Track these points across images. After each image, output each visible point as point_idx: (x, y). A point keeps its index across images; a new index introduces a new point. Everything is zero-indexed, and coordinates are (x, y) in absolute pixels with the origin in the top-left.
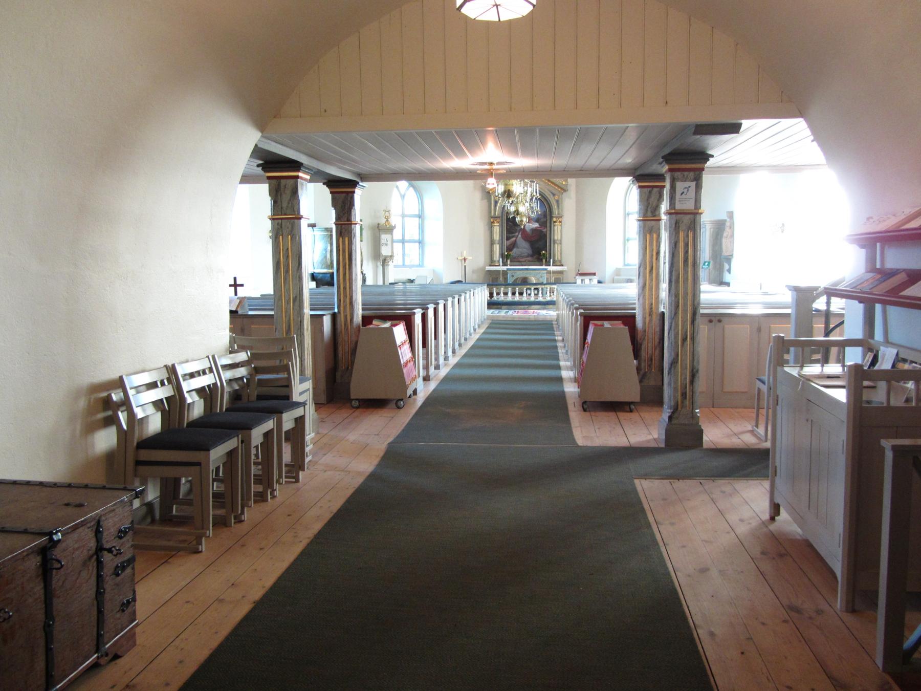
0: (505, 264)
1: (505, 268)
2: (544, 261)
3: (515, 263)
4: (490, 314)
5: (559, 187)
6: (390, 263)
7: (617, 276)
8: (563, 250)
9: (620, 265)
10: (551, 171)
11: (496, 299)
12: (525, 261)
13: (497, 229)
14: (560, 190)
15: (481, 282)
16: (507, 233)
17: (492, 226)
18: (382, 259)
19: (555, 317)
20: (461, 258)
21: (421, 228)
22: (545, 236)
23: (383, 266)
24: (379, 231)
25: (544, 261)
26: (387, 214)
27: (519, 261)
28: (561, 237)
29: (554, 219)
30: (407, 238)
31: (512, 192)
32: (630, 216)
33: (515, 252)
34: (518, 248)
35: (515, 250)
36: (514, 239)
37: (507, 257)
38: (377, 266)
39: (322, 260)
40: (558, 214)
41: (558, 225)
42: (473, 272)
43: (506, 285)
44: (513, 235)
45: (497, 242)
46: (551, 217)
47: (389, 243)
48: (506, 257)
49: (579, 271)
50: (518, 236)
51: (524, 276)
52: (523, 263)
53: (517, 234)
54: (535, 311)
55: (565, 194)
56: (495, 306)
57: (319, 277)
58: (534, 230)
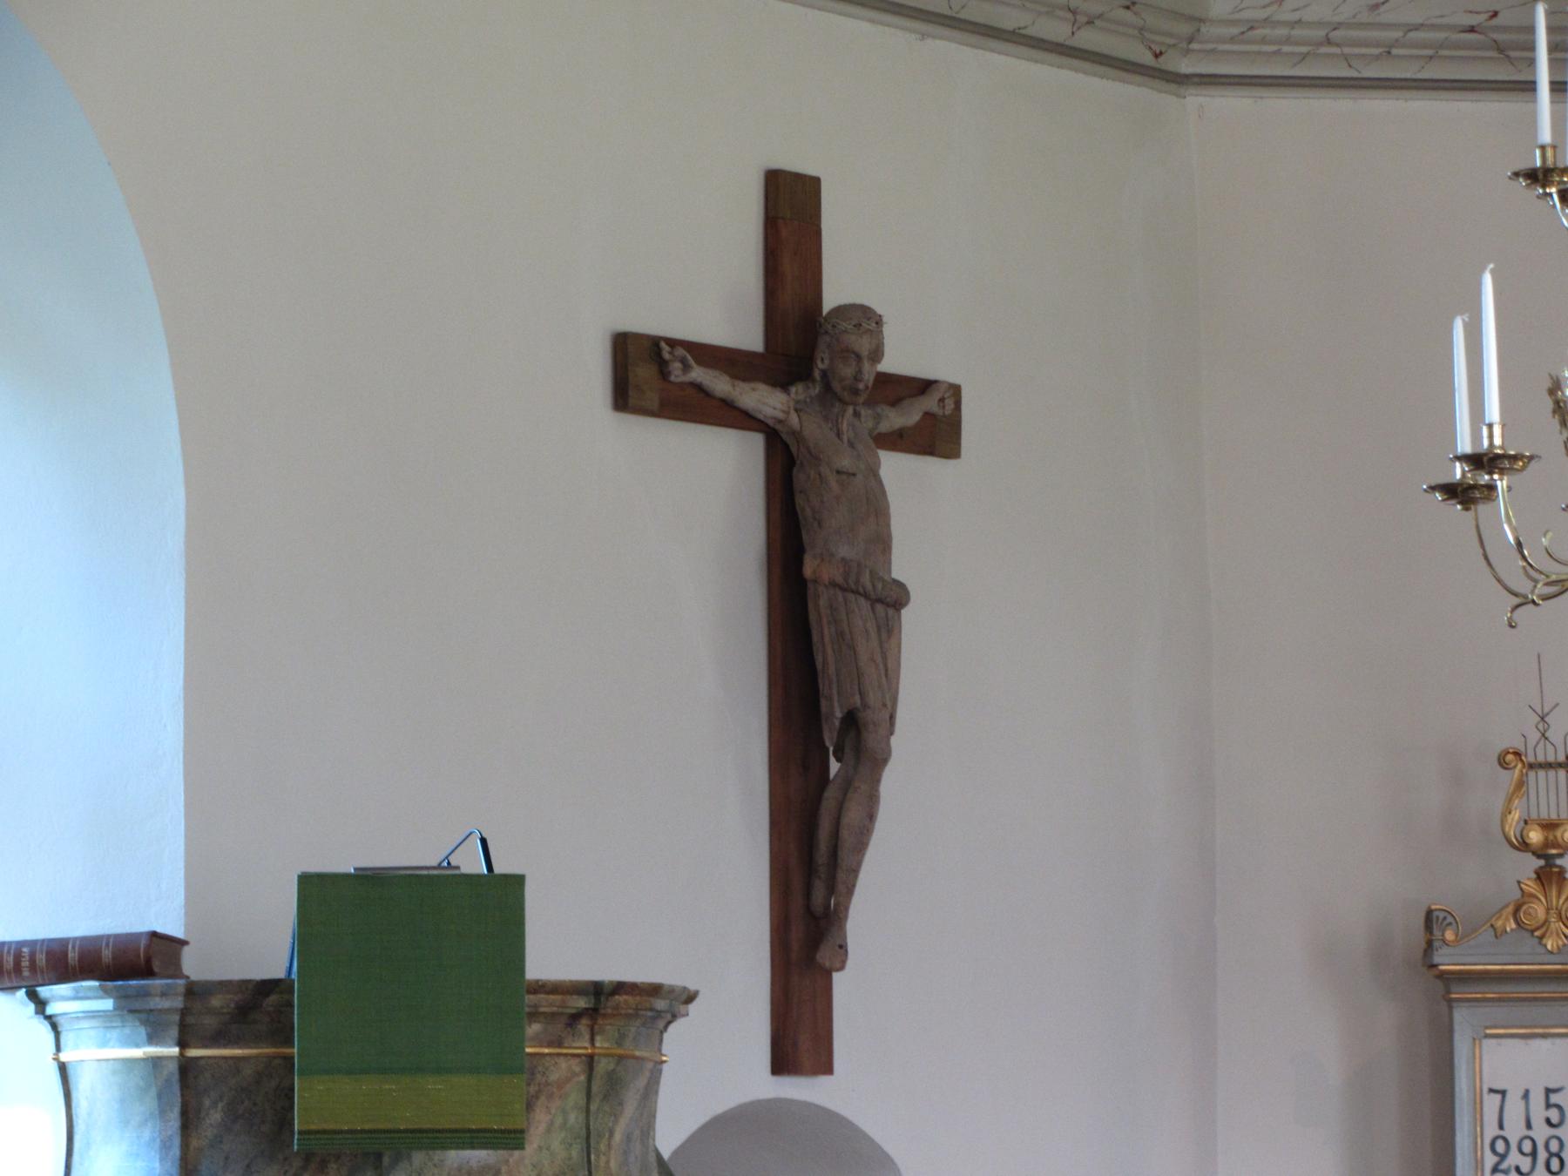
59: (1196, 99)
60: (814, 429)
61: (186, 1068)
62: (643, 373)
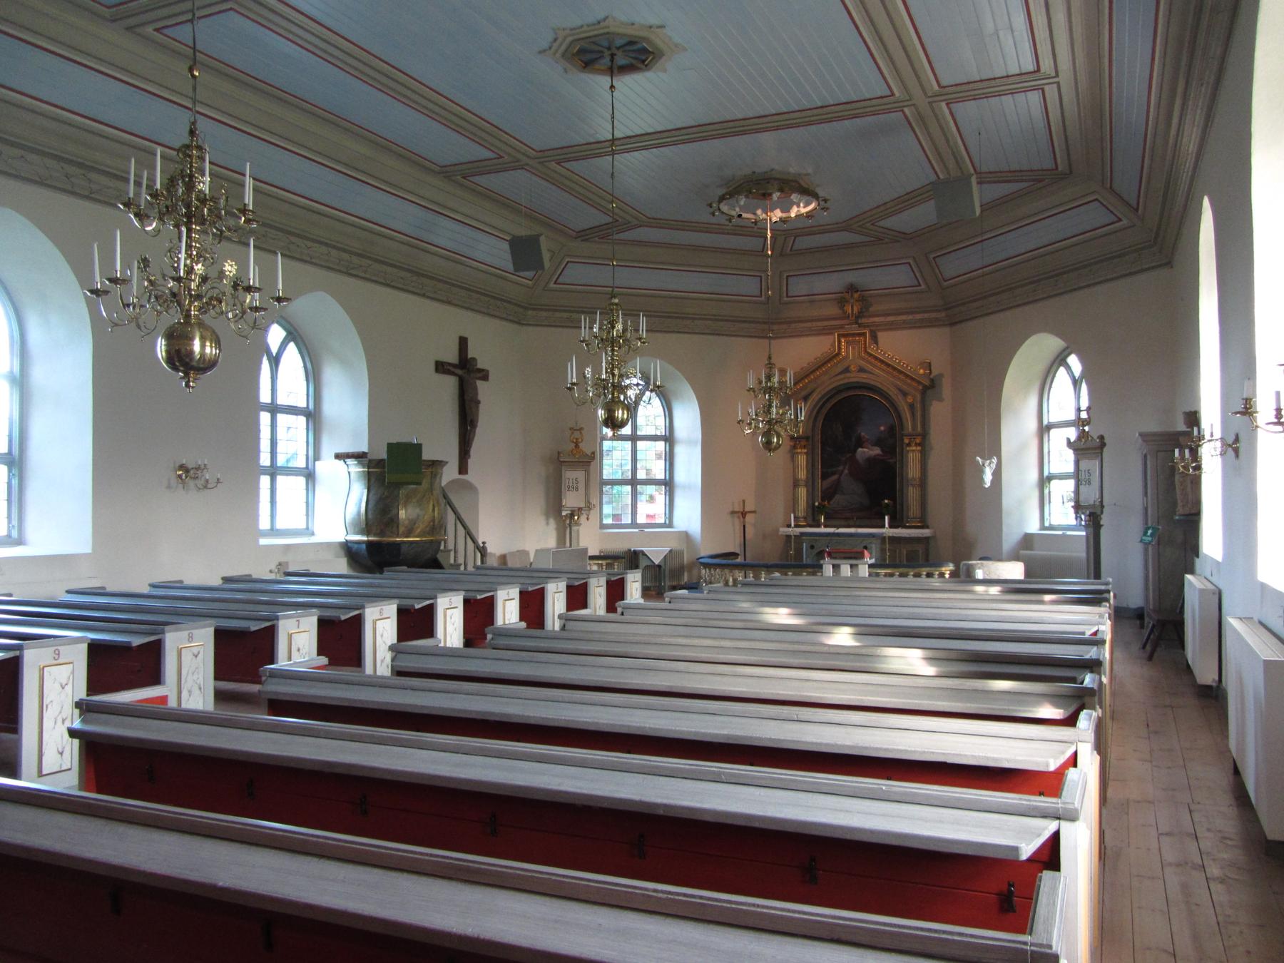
9: (1033, 527)
14: (909, 381)
21: (670, 459)
26: (577, 434)
35: (837, 497)
36: (835, 477)
44: (834, 469)
50: (842, 471)
53: (841, 468)
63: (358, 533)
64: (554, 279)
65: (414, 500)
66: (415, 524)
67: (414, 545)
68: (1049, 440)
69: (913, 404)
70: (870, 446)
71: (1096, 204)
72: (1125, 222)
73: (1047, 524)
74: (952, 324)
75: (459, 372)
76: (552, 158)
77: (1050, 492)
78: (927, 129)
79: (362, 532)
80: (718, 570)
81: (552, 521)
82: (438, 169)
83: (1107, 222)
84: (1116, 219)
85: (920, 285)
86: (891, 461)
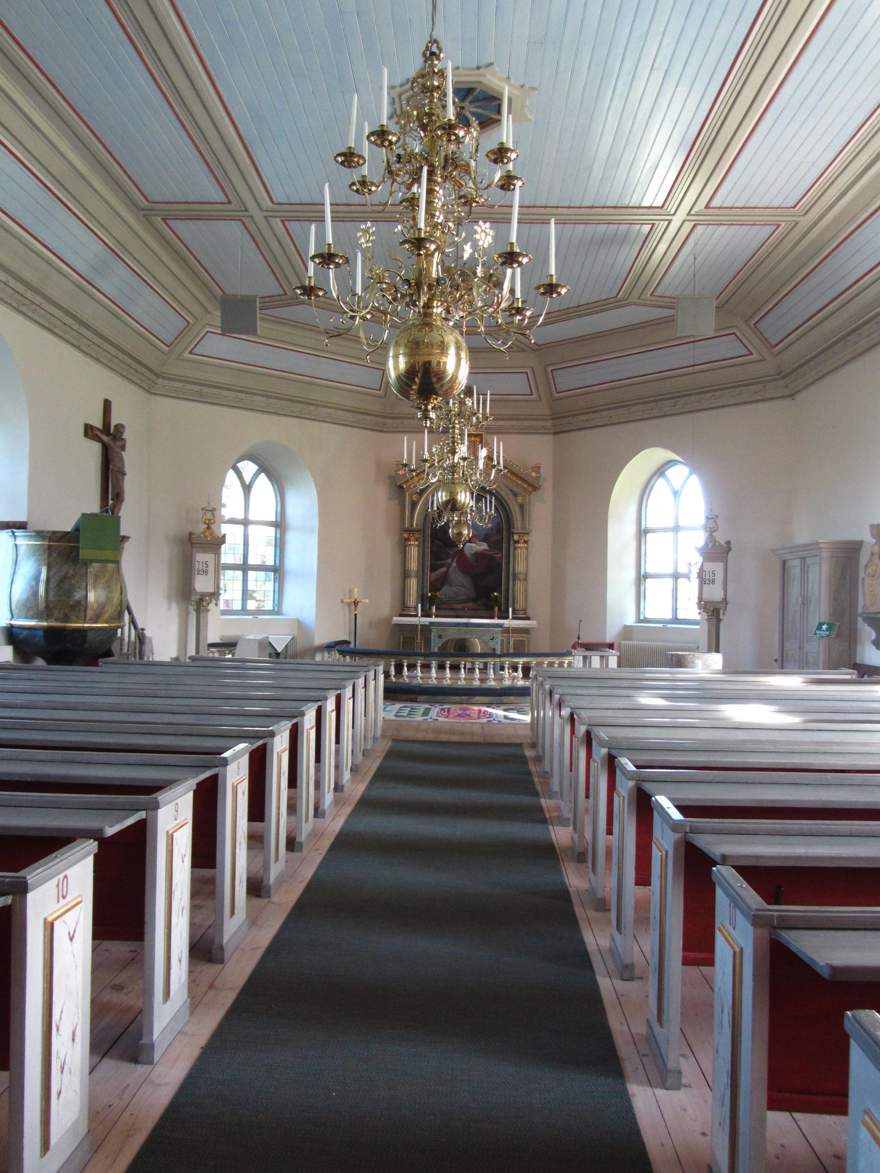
0: (426, 614)
1: (426, 620)
2: (496, 609)
3: (443, 613)
4: (391, 717)
5: (525, 481)
6: (212, 606)
7: (625, 639)
8: (529, 591)
9: (630, 620)
10: (211, 986)
11: (407, 680)
12: (463, 609)
13: (414, 552)
15: (382, 647)
16: (431, 560)
17: (405, 546)
18: (194, 598)
19: (527, 732)
20: (349, 600)
21: (280, 545)
22: (500, 565)
23: (198, 611)
24: (192, 547)
25: (496, 609)
26: (209, 515)
27: (452, 609)
28: (527, 570)
29: (516, 537)
30: (252, 561)
31: (440, 375)
32: (648, 535)
33: (445, 592)
34: (451, 585)
35: (445, 589)
36: (444, 569)
37: (432, 601)
38: (188, 613)
39: (28, 599)
40: (523, 528)
41: (521, 548)
42: (371, 625)
43: (429, 655)
44: (443, 562)
45: (413, 574)
46: (510, 534)
47: (211, 569)
48: (428, 603)
49: (579, 638)
50: (451, 564)
51: (461, 637)
52: (459, 613)
53: (449, 561)
54: (483, 709)
55: (534, 493)
56: (405, 697)
57: (22, 636)
58: (479, 555)
59: (153, 397)
60: (111, 443)
61: (50, 547)
62: (89, 431)
63: (27, 618)
64: (190, 349)
65: (103, 581)
66: (104, 608)
67: (100, 631)
68: (646, 543)
69: (523, 505)
70: (478, 542)
71: (733, 337)
72: (755, 356)
73: (642, 618)
74: (555, 433)
75: (105, 438)
76: (279, 214)
77: (645, 589)
78: (73, 282)
79: (38, 616)
80: (348, 657)
81: (174, 606)
82: (143, 203)
83: (741, 354)
84: (748, 352)
85: (532, 395)
86: (497, 556)
